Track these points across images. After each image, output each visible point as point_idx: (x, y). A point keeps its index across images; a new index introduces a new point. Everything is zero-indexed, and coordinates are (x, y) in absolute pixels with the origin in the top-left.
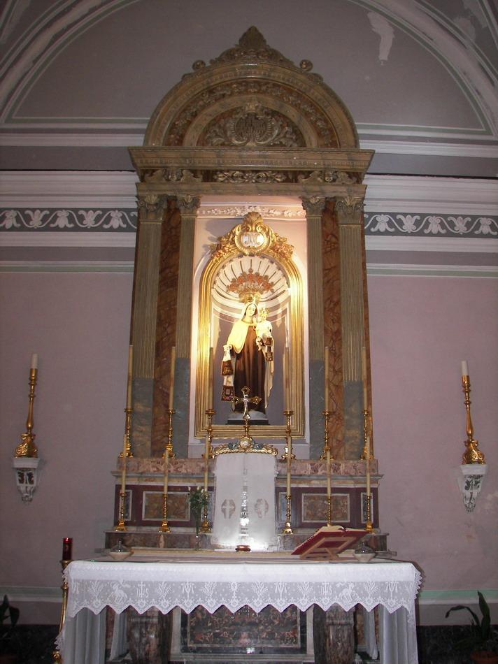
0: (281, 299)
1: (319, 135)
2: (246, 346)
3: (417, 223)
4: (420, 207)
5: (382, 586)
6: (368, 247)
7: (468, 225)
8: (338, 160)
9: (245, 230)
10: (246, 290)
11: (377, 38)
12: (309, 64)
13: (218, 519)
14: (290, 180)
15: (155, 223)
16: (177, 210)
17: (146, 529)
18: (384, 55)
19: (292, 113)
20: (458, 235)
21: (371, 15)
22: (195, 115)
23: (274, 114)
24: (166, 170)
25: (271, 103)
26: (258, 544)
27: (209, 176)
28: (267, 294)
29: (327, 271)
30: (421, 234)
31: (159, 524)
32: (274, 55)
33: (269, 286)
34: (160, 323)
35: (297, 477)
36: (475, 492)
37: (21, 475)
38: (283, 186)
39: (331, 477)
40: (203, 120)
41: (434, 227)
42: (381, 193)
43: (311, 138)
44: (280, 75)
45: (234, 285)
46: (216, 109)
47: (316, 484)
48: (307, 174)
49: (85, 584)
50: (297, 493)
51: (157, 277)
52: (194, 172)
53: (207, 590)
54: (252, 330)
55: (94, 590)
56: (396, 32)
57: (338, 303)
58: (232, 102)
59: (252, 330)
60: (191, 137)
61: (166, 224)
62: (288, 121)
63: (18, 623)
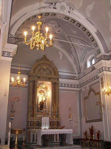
0: (46, 95)
1: (54, 73)
2: (42, 101)
3: (64, 85)
4: (32, 14)
5: (70, 131)
6: (59, 88)
7: (71, 86)
8: (56, 77)
9: (42, 85)
10: (40, 92)
11: (60, 56)
12: (52, 62)
13: (42, 125)
14: (49, 79)
15: (31, 84)
16: (35, 82)
17: (32, 127)
18: (61, 58)
19: (50, 69)
20: (69, 87)
21: (59, 52)
22: (37, 68)
23: (48, 69)
24: (33, 76)
25: (47, 67)
26: (47, 128)
27: (39, 78)
28: (43, 93)
29: (54, 92)
30: (65, 87)
31: (34, 126)
32: (48, 60)
33: (44, 92)
34: (32, 98)
35: (51, 120)
36: (70, 122)
37: (11, 119)
38: (48, 80)
39: (55, 120)
40: (38, 69)
41: (67, 86)
42: (61, 80)
43: (53, 74)
44: (49, 63)
45: (39, 91)
46: (40, 67)
47: (53, 121)
48: (52, 78)
49: (43, 132)
50: (51, 122)
51: (32, 92)
52: (37, 77)
53: (50, 132)
54: (42, 99)
55: (44, 132)
56: (63, 55)
57: (55, 97)
58: (42, 66)
59: (42, 99)
60: (36, 71)
61: (33, 84)
62: (21, 27)
63: (13, 140)
